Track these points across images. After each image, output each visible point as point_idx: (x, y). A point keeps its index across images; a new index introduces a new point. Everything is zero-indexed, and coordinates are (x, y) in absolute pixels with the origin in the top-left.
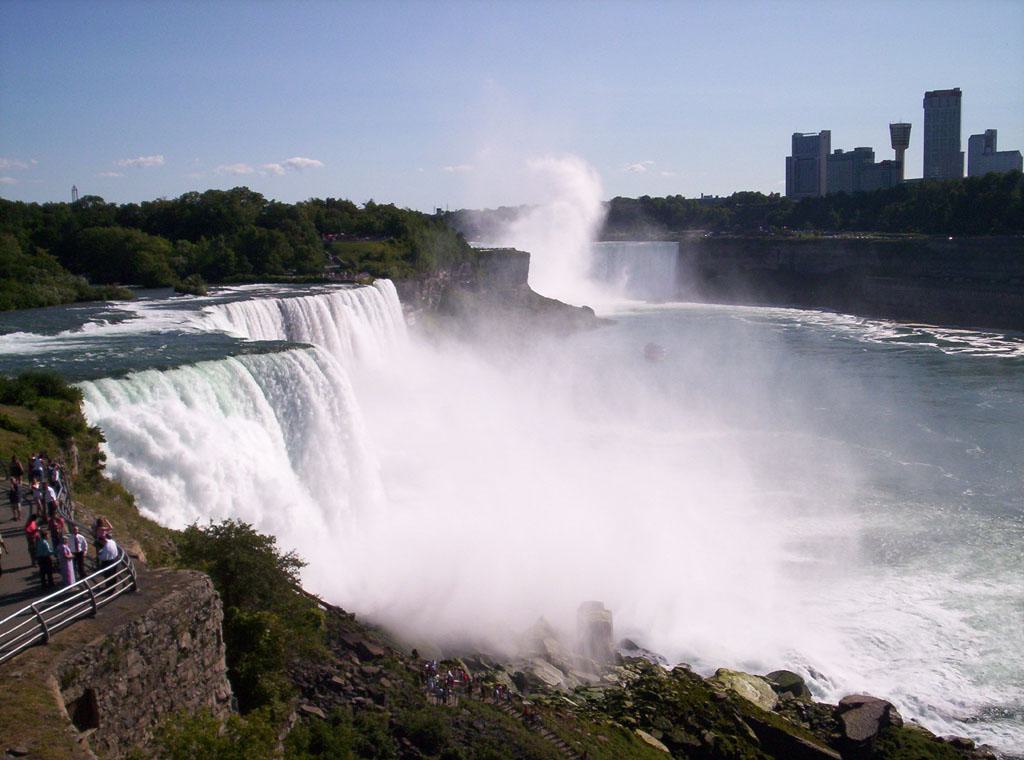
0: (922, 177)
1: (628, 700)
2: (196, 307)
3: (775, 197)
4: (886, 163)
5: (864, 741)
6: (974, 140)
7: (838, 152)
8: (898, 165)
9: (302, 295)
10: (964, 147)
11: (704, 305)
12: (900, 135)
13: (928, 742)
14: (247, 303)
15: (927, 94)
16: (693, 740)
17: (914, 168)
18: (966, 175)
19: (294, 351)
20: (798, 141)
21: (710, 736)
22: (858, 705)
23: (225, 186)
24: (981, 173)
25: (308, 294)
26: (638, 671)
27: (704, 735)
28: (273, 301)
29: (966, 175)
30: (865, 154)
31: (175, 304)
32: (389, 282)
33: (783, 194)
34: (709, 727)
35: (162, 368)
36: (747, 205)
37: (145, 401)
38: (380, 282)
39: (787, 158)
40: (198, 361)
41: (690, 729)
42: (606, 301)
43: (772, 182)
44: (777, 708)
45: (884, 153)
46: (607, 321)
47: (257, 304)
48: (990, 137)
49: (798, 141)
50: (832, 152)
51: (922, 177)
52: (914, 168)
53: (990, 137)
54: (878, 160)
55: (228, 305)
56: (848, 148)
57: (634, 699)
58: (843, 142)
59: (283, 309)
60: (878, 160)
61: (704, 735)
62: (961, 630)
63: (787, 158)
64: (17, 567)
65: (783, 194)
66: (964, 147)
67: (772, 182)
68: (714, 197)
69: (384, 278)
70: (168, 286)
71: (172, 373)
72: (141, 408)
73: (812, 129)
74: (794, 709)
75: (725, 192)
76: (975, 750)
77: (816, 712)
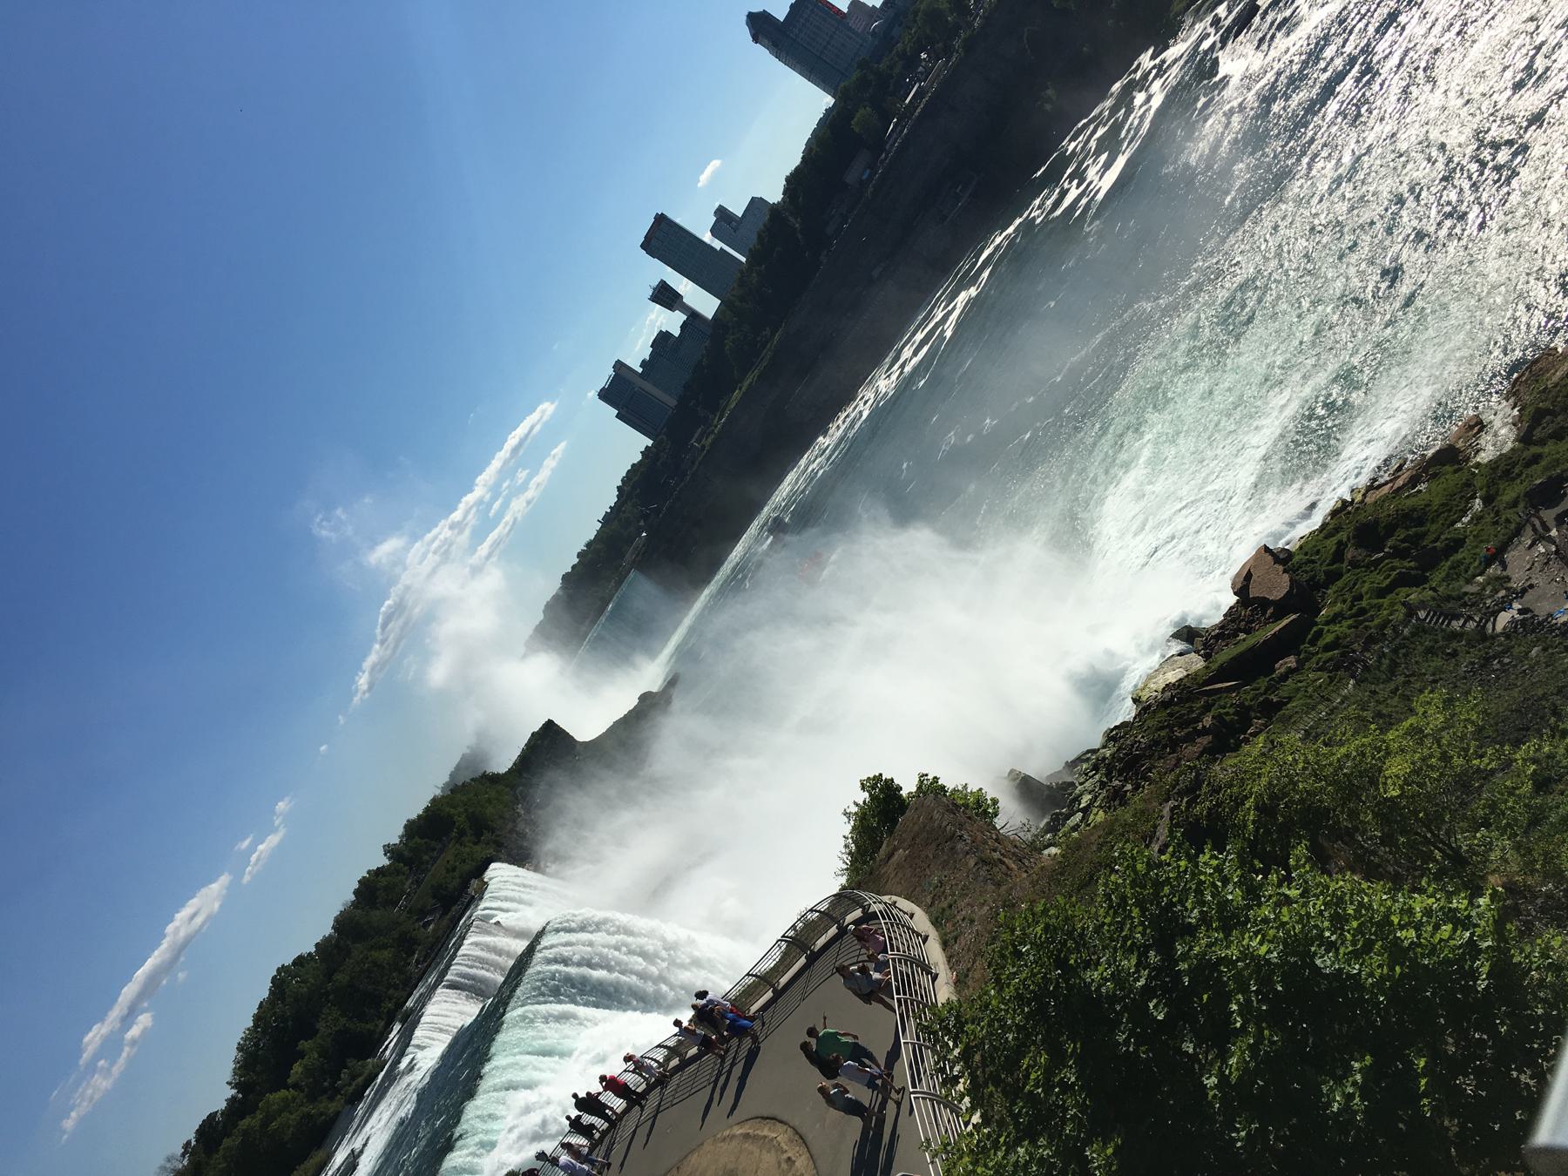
0: (828, 101)
1: (1123, 786)
2: (392, 1078)
3: (647, 452)
4: (684, 326)
5: (1291, 587)
6: (715, 231)
7: (644, 364)
8: (693, 316)
9: (454, 956)
10: (717, 244)
11: (706, 592)
12: (665, 296)
13: (1322, 535)
14: (423, 1020)
15: (643, 246)
16: (1204, 741)
17: (706, 304)
18: (743, 259)
19: (538, 947)
20: (605, 395)
21: (1207, 721)
22: (1249, 576)
23: (262, 990)
24: (753, 240)
25: (457, 950)
26: (1091, 774)
27: (1204, 727)
28: (439, 990)
29: (743, 259)
30: (663, 339)
31: (370, 1104)
32: (493, 866)
33: (650, 442)
34: (1198, 719)
35: (470, 1094)
36: (638, 484)
37: (498, 1131)
38: (489, 874)
39: (617, 417)
40: (488, 1048)
41: (1190, 738)
42: (650, 674)
43: (631, 445)
44: (1207, 657)
45: (672, 322)
46: (672, 683)
47: (431, 1010)
48: (722, 213)
49: (605, 395)
50: (640, 370)
51: (828, 101)
52: (706, 304)
53: (722, 213)
54: (676, 332)
55: (412, 1043)
56: (646, 353)
57: (1126, 780)
58: (636, 354)
59: (453, 986)
60: (676, 332)
61: (1204, 727)
62: (1355, 244)
63: (617, 417)
64: (784, 1119)
65: (650, 442)
66: (717, 244)
67: (631, 445)
68: (609, 511)
69: (487, 868)
70: (338, 1114)
71: (485, 1085)
72: (505, 1139)
73: (604, 376)
74: (1217, 641)
75: (612, 498)
76: (1353, 500)
77: (1233, 621)
